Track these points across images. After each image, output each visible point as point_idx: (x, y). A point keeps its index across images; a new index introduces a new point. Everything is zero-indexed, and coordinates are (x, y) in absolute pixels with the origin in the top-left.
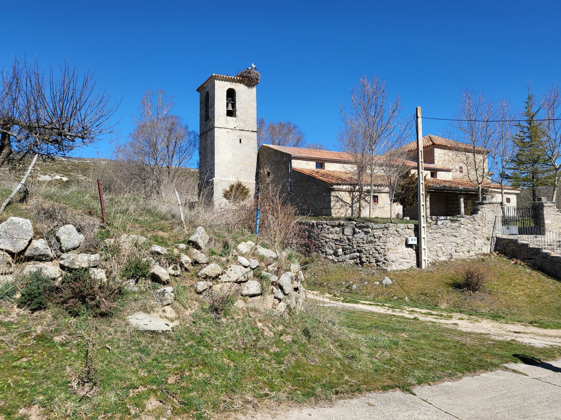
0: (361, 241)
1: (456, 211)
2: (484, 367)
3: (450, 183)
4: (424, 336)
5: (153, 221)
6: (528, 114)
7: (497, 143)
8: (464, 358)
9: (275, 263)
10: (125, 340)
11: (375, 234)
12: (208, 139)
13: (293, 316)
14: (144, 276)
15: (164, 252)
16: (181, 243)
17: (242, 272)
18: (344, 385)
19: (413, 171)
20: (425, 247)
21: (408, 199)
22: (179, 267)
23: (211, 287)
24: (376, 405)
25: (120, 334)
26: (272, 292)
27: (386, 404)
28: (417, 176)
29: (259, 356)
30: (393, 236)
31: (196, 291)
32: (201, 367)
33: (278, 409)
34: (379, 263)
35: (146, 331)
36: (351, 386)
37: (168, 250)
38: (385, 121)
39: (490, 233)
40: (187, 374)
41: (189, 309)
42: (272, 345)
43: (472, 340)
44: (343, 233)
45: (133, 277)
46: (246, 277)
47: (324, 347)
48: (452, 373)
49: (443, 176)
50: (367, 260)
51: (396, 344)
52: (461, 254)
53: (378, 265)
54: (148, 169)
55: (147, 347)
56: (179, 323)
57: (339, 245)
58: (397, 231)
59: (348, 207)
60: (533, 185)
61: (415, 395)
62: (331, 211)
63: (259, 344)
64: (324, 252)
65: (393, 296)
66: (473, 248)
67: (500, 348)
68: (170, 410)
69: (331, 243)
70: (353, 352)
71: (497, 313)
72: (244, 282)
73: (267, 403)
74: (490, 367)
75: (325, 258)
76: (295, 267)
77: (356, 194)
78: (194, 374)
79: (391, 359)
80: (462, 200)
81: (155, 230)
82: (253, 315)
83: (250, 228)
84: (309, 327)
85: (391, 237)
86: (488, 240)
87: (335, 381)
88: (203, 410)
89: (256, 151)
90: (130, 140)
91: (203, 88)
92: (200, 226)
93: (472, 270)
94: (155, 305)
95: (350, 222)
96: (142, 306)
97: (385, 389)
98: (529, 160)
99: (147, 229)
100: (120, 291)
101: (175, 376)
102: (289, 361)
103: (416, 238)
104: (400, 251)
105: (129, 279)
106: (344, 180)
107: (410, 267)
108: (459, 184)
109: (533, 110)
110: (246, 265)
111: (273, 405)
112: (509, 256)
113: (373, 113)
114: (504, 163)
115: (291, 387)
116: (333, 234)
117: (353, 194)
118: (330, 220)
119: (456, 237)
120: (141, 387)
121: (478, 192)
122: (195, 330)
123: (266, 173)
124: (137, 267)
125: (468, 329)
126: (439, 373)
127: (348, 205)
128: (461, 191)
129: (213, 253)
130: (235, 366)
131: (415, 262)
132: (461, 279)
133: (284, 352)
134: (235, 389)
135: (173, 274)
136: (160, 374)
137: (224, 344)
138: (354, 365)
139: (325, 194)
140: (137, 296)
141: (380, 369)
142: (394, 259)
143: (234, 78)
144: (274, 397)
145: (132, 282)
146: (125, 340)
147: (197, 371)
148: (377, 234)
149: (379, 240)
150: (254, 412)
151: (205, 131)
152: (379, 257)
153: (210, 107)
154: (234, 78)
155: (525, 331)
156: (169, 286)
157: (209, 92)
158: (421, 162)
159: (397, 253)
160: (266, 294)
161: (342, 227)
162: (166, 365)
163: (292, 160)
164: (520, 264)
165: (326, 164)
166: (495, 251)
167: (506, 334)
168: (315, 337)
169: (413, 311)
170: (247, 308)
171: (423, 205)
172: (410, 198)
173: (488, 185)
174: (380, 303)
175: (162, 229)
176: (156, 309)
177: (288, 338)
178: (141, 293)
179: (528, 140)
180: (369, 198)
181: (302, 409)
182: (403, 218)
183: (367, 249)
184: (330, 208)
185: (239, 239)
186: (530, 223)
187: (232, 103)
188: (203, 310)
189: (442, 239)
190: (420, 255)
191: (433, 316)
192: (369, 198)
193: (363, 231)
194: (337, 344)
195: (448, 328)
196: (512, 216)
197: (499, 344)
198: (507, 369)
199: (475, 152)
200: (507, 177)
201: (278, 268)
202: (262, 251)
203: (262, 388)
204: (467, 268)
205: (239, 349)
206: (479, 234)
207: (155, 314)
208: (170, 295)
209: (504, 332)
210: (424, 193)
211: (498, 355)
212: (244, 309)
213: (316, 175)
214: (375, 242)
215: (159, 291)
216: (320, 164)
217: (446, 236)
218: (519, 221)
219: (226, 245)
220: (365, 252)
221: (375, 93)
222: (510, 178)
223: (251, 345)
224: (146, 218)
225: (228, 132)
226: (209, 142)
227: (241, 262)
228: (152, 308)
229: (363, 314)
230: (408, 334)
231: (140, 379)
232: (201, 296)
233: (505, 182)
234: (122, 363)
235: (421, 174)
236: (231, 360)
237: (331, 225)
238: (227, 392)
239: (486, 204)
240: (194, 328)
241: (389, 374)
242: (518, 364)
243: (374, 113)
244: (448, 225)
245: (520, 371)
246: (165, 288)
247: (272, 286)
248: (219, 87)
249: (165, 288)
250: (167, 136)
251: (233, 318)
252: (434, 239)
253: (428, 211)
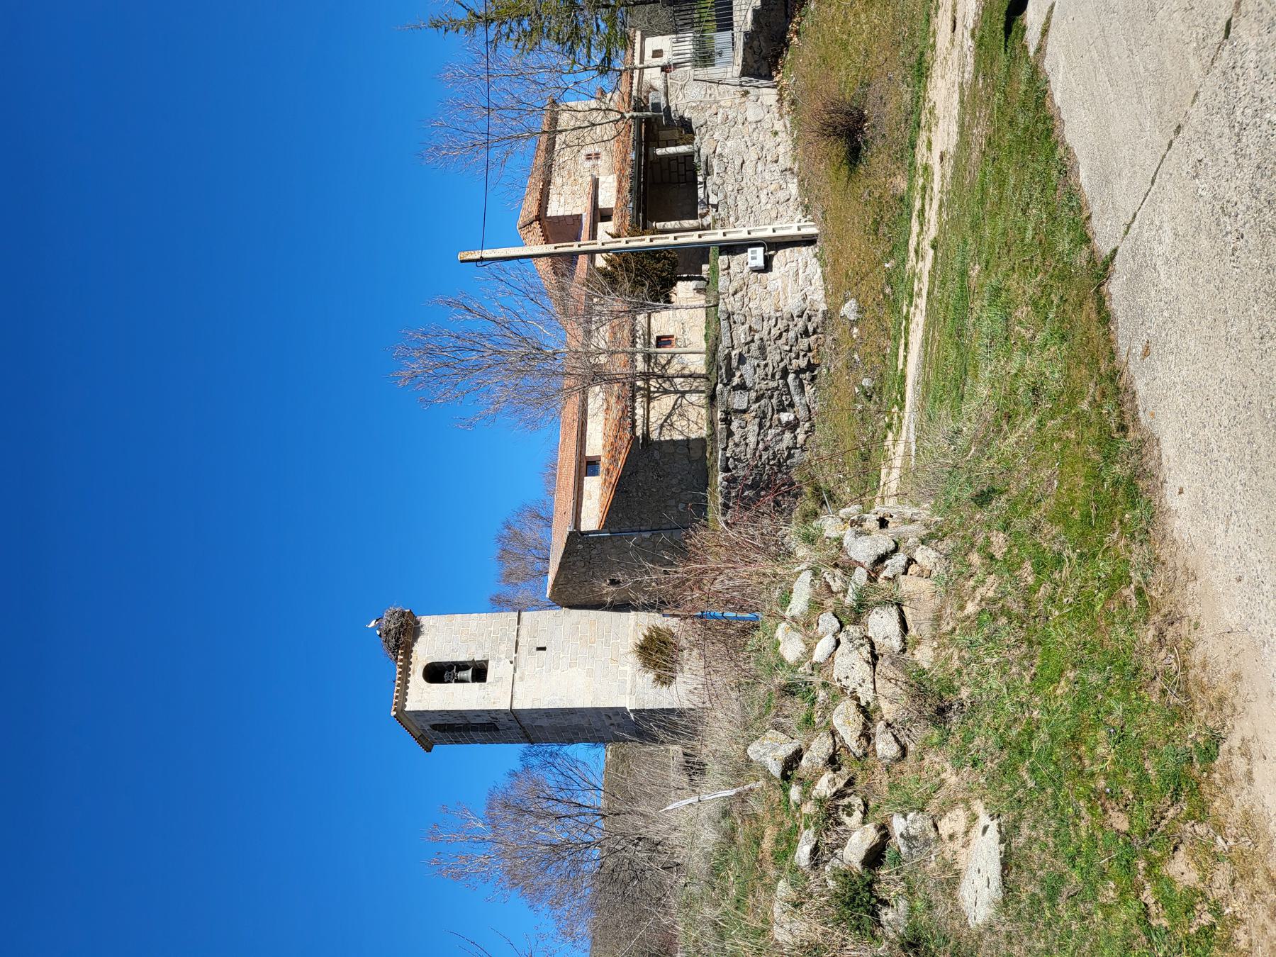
0: (760, 372)
1: (685, 163)
2: (1038, 98)
3: (624, 179)
4: (975, 227)
5: (739, 861)
6: (470, 27)
7: (533, 86)
8: (1020, 142)
9: (825, 575)
10: (1029, 934)
11: (743, 341)
12: (538, 723)
13: (945, 530)
14: (870, 885)
15: (811, 836)
16: (788, 796)
17: (851, 652)
18: (1104, 412)
19: (600, 262)
20: (770, 228)
21: (662, 272)
22: (846, 801)
23: (888, 725)
24: (1145, 338)
25: (1016, 948)
26: (893, 579)
27: (1142, 315)
28: (611, 254)
29: (1046, 608)
30: (746, 300)
31: (898, 760)
32: (1083, 748)
33: (1171, 565)
34: (811, 329)
35: (1004, 883)
36: (1103, 395)
37: (807, 827)
38: (492, 328)
39: (732, 91)
40: (1102, 783)
41: (943, 776)
42: (1017, 580)
43: (979, 123)
44: (744, 411)
45: (874, 913)
46: (862, 641)
47: (1015, 456)
48: (1059, 167)
49: (608, 194)
50: (804, 356)
51: (997, 292)
52: (781, 149)
53: (815, 332)
54: (610, 862)
55: (1043, 881)
56: (979, 800)
57: (771, 419)
58: (735, 293)
59: (684, 401)
60: (622, 6)
61: (1115, 251)
62: (693, 440)
63: (1017, 608)
64: (789, 453)
65: (885, 295)
66: (767, 125)
67: (992, 63)
68: (1196, 827)
69: (769, 438)
70: (1021, 389)
71: (912, 67)
72: (872, 645)
73: (1160, 590)
74: (1038, 84)
75: (803, 451)
76: (830, 525)
77: (654, 384)
78: (1101, 766)
79: (1035, 304)
80: (659, 152)
81: (760, 857)
82: (948, 624)
83: (744, 632)
84: (968, 493)
85: (751, 306)
86: (747, 93)
87: (1094, 431)
88: (1189, 745)
89: (564, 611)
90: (544, 907)
91: (424, 738)
92: (745, 751)
93: (816, 126)
94: (939, 859)
95: (719, 397)
96: (944, 891)
97: (1105, 318)
98: (568, 17)
99: (760, 878)
100: (911, 945)
101: (1110, 812)
102: (1051, 537)
103: (750, 250)
105: (879, 921)
106: (623, 412)
107: (815, 260)
108: (624, 160)
109: (462, 15)
110: (833, 642)
111: (1163, 578)
112: (782, 49)
113: (474, 356)
114: (576, 67)
115: (1115, 535)
116: (747, 432)
117: (654, 392)
118: (714, 441)
119: (744, 162)
120: (1142, 898)
121: (641, 118)
122: (992, 761)
123: (612, 588)
124: (851, 902)
125: (951, 130)
126: (1060, 197)
127: (679, 402)
128: (639, 155)
129: (808, 720)
130: (1074, 666)
131: (804, 249)
132: (839, 149)
133: (1031, 549)
134: (1130, 668)
135: (861, 816)
136: (1108, 851)
137: (1022, 694)
138: (1052, 387)
139: (657, 455)
140: (918, 904)
141: (1060, 328)
142: (799, 296)
143: (400, 667)
144: (1144, 576)
145: (886, 914)
146: (1029, 934)
147: (1094, 760)
148: (743, 336)
149: (756, 331)
150: (1185, 622)
151: (521, 731)
152: (796, 329)
153: (464, 722)
154: (400, 667)
155: (950, 8)
156: (890, 823)
157: (433, 723)
158: (579, 246)
159: (784, 289)
160: (899, 594)
161: (729, 413)
162: (1083, 833)
163: (582, 530)
164: (799, 24)
165: (589, 453)
166: (770, 78)
167: (959, 48)
168: (993, 479)
169: (916, 252)
170: (934, 637)
171: (675, 238)
172: (660, 265)
173: (626, 99)
174: (901, 324)
175: (758, 841)
176: (948, 856)
177: (999, 542)
178: (911, 891)
179: (526, 23)
180: (663, 355)
181: (1169, 509)
182: (704, 279)
183: (778, 358)
184: (688, 440)
185: (773, 660)
186: (707, 8)
187: (457, 671)
188: (944, 741)
189: (750, 193)
190: (787, 240)
191: (927, 207)
192: (663, 355)
193: (738, 368)
194: (1006, 427)
195: (953, 174)
196: (691, 47)
197: (982, 66)
198: (1040, 49)
199: (554, 130)
200: (607, 60)
201: (836, 566)
202: (798, 604)
203: (1125, 604)
204: (811, 137)
205: (1032, 657)
206: (734, 114)
207: (961, 859)
208: (913, 822)
209: (956, 53)
210: (648, 238)
211: (1008, 67)
212: (935, 644)
213: (615, 474)
214: (762, 339)
215: (904, 849)
216: (588, 466)
217: (743, 184)
218: (704, 31)
219: (789, 690)
220: (786, 361)
221: (430, 353)
222: (610, 54)
223: (1021, 627)
224: (732, 879)
225: (522, 679)
226: (544, 722)
227: (826, 655)
228: (946, 866)
229: (930, 363)
230: (972, 264)
231: (1125, 901)
232: (911, 747)
233: (618, 64)
234: (1087, 944)
235: (607, 247)
236: (1060, 676)
237: (728, 439)
238: (1140, 688)
239: (667, 102)
240: (989, 764)
241: (1069, 308)
242: (1028, 25)
243: (474, 353)
244: (719, 181)
245: (1043, 20)
246: (897, 834)
247: (879, 580)
248: (420, 701)
249: (897, 834)
250: (533, 819)
251: (959, 671)
252: (749, 210)
253: (687, 223)
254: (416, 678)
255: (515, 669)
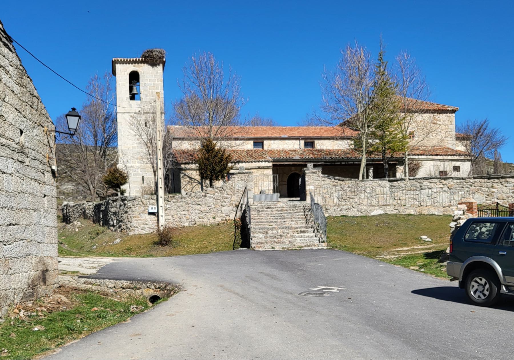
104: (143, 218)
165: (316, 142)
248: (120, 71)
254: (131, 68)
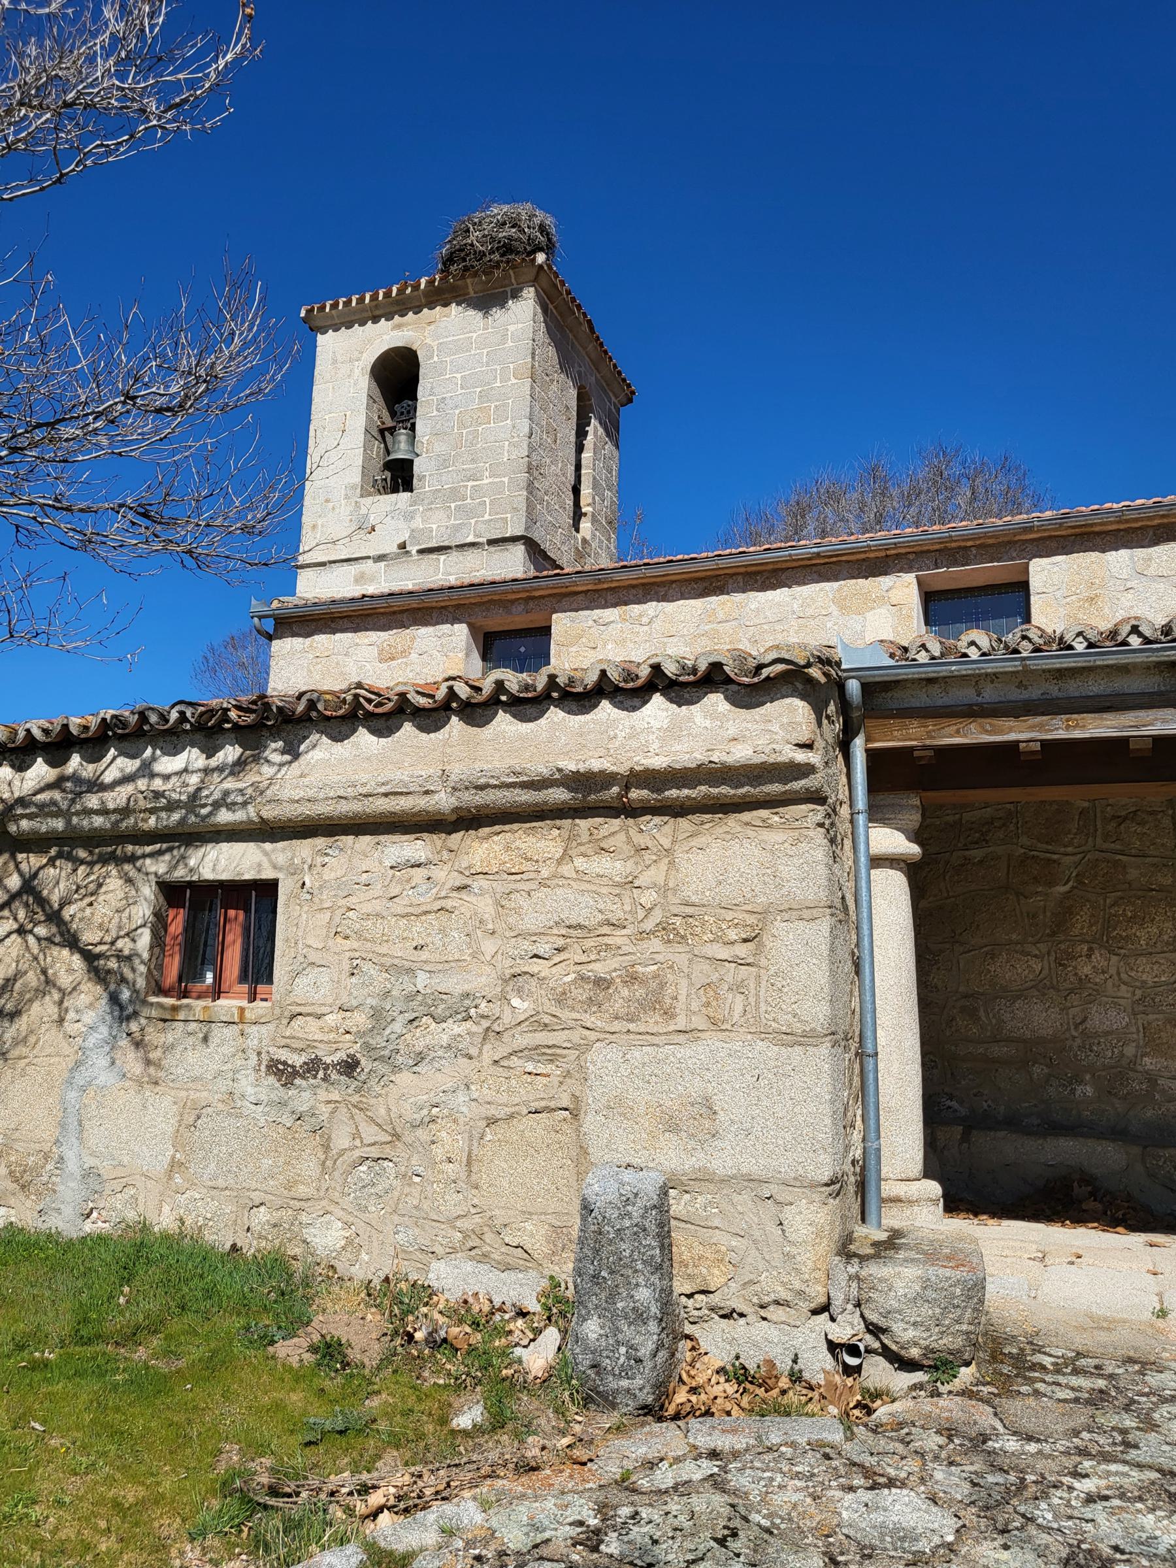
248: (335, 361)
255: (380, 558)
